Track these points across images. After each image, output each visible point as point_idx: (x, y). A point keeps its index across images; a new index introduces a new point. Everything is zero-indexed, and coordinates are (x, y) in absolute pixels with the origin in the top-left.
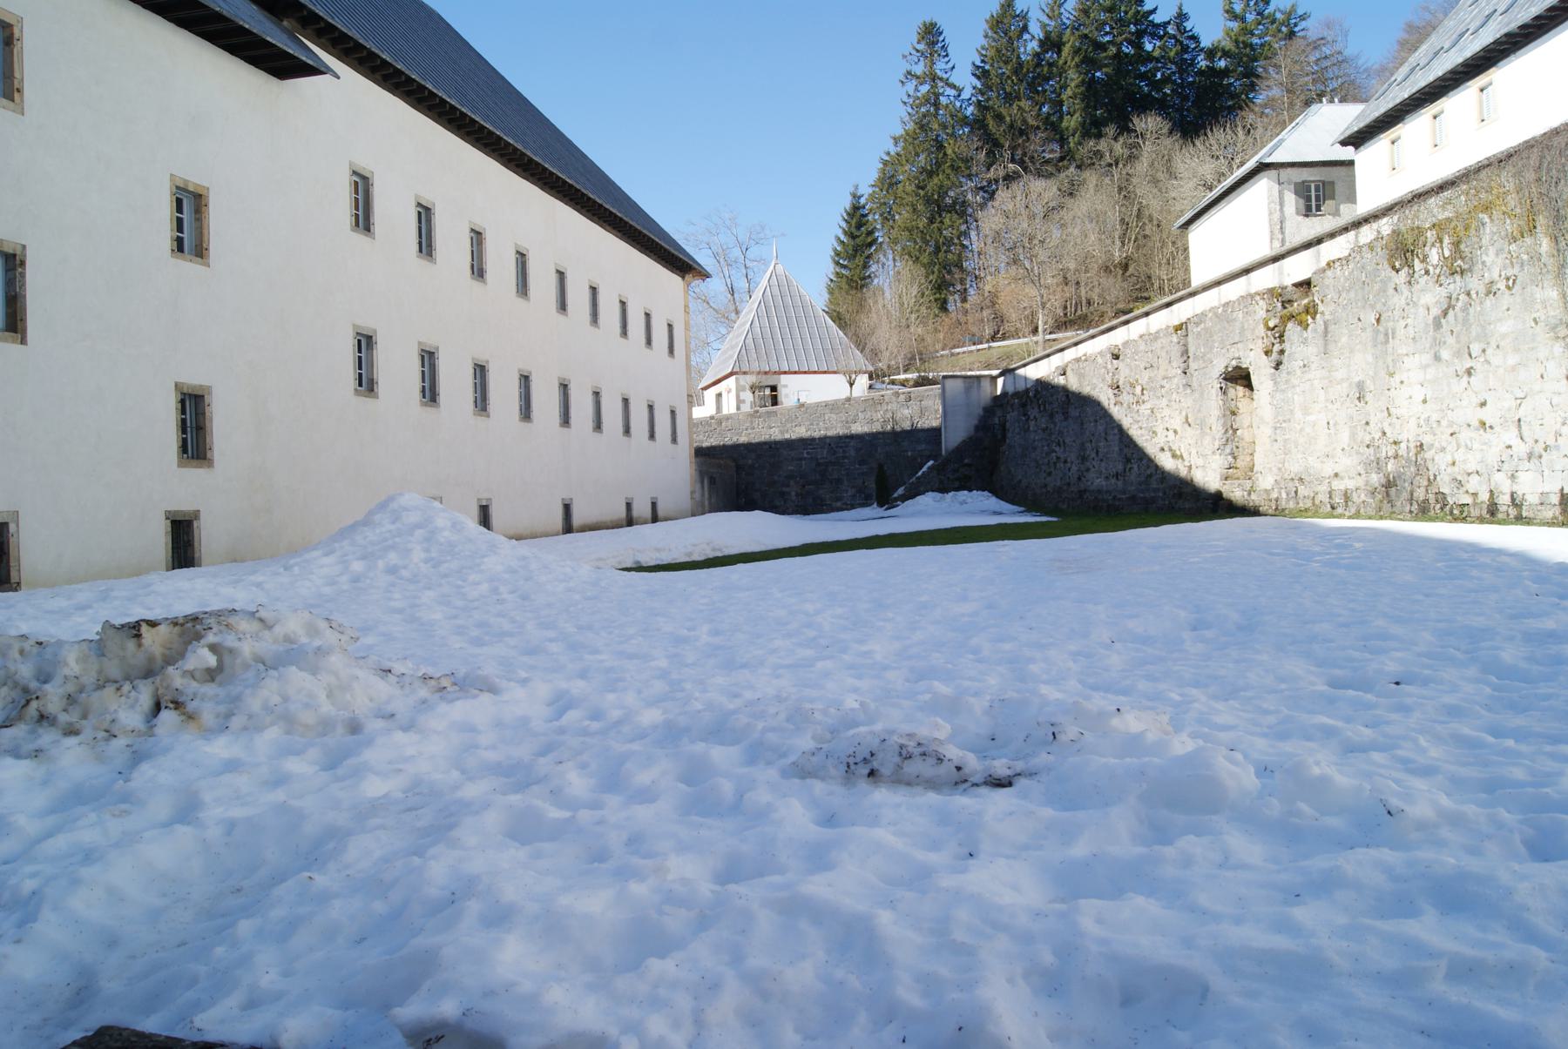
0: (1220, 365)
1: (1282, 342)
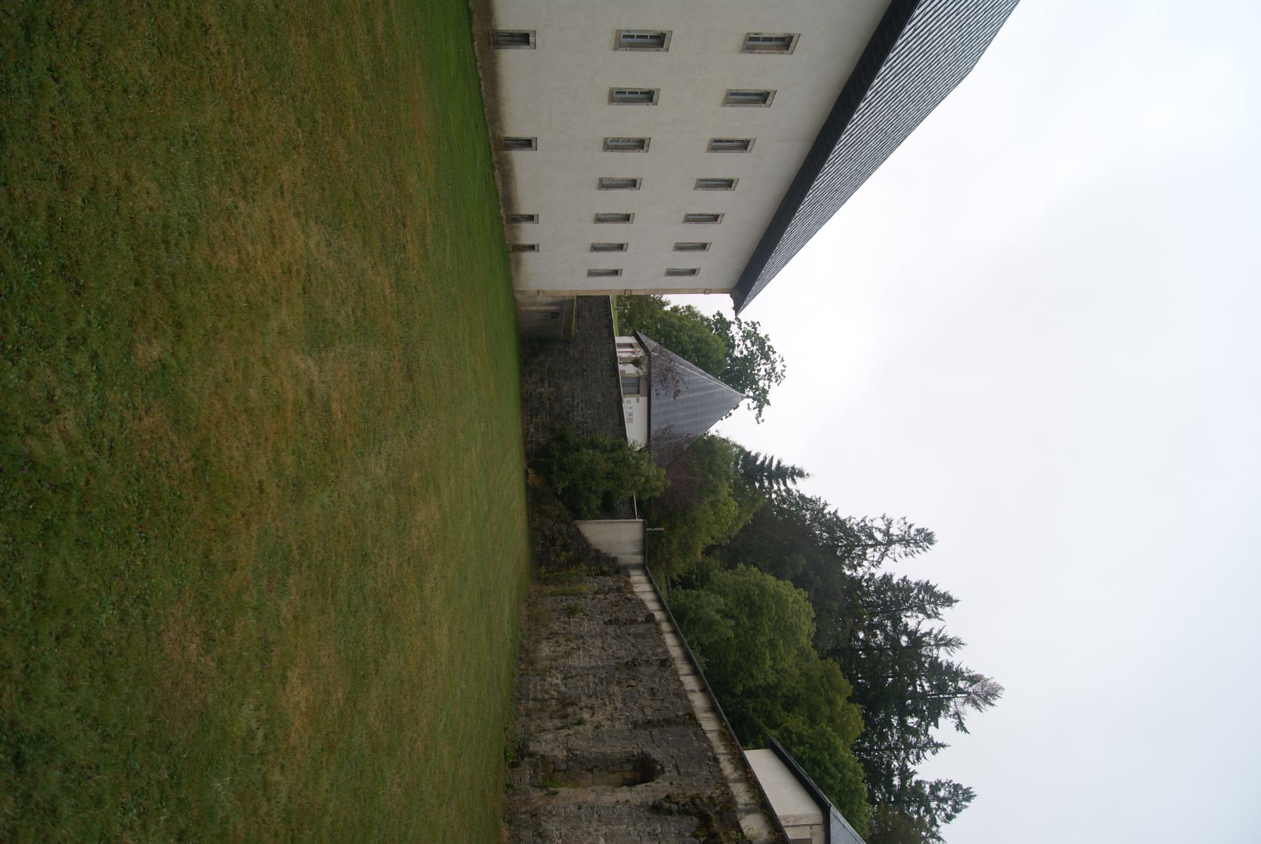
0: (657, 754)
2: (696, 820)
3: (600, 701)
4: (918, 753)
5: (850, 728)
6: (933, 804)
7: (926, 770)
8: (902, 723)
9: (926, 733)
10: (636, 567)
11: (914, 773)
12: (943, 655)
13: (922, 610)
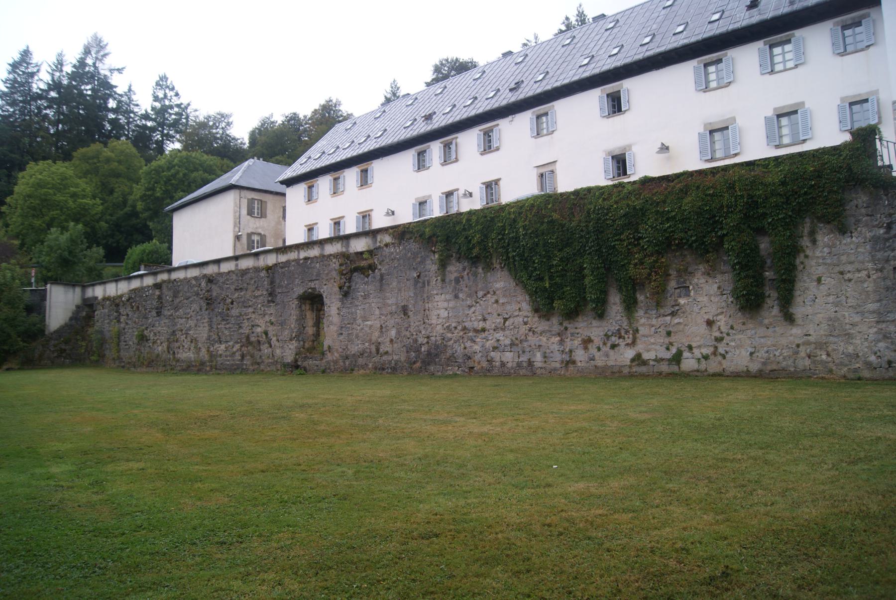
1: (350, 282)
2: (355, 274)
3: (245, 321)
4: (134, 105)
5: (128, 150)
6: (167, 103)
7: (144, 103)
8: (114, 111)
9: (121, 96)
10: (83, 292)
11: (146, 111)
12: (68, 69)
13: (32, 75)
